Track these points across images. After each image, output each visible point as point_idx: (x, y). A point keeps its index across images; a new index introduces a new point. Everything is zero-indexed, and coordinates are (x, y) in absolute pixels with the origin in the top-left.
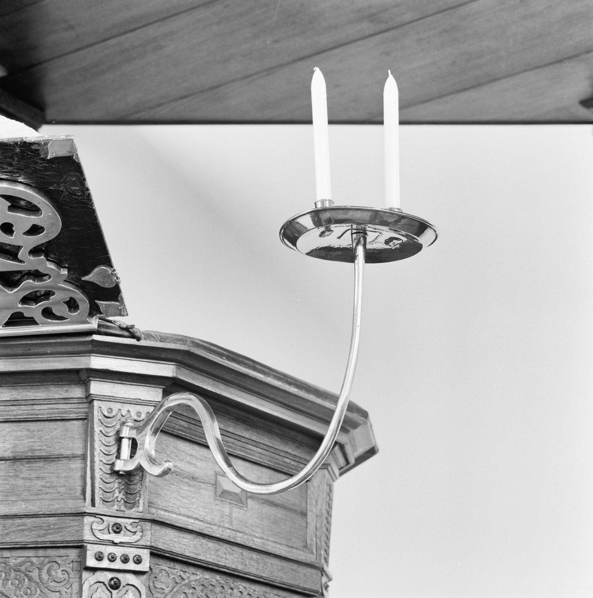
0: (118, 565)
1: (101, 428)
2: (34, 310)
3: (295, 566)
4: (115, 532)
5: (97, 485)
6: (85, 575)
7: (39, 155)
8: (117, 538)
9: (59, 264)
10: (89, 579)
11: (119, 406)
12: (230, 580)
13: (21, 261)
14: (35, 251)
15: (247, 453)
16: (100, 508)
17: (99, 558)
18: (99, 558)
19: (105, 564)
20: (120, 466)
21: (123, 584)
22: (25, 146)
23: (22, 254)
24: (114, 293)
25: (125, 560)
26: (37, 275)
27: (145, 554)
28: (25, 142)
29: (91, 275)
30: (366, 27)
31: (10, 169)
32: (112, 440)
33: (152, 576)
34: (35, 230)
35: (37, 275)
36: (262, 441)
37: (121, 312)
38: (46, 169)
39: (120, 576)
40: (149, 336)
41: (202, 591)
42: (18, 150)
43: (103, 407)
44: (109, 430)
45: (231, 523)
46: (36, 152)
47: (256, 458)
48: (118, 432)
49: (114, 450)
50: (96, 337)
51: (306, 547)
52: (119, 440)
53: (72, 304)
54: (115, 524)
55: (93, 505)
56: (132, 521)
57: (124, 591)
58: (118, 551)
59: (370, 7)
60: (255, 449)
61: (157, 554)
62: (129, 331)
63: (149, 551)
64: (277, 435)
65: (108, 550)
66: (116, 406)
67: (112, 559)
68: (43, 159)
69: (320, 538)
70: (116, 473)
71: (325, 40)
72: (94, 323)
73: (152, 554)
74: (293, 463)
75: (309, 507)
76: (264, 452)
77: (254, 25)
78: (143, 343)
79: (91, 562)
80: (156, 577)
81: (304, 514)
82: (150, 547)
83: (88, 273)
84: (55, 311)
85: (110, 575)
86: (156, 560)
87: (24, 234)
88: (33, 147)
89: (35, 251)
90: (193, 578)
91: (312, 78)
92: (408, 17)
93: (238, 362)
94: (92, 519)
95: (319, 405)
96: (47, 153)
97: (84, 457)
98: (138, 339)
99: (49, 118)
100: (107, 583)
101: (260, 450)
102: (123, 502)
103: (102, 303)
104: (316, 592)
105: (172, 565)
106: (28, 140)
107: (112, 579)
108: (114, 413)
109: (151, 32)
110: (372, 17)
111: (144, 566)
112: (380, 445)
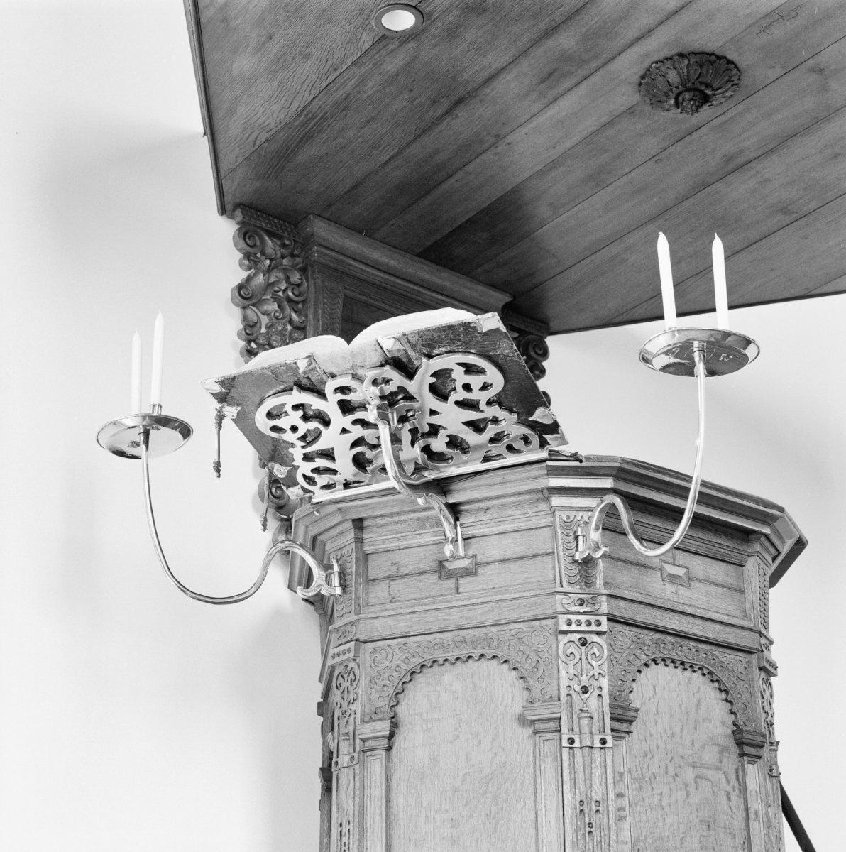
0: (583, 628)
1: (563, 531)
2: (500, 448)
3: (735, 630)
4: (580, 605)
5: (563, 571)
6: (560, 637)
7: (476, 330)
8: (582, 609)
9: (511, 411)
10: (563, 639)
11: (574, 513)
12: (679, 640)
13: (482, 411)
14: (489, 403)
15: (686, 545)
16: (566, 588)
17: (569, 624)
18: (569, 624)
19: (574, 627)
20: (578, 557)
21: (589, 642)
22: (466, 325)
23: (482, 405)
24: (554, 428)
25: (589, 624)
26: (495, 421)
27: (604, 619)
28: (465, 323)
29: (534, 416)
30: (781, 219)
31: (459, 343)
32: (572, 538)
33: (612, 636)
34: (485, 387)
35: (495, 421)
36: (697, 535)
37: (564, 442)
38: (484, 340)
39: (586, 636)
40: (588, 458)
41: (656, 647)
42: (462, 329)
43: (563, 515)
44: (568, 531)
45: (678, 598)
46: (475, 329)
47: (694, 549)
48: (575, 532)
49: (574, 545)
50: (549, 463)
51: (746, 616)
52: (577, 538)
53: (526, 440)
54: (579, 599)
55: (562, 586)
56: (592, 596)
57: (590, 647)
58: (583, 618)
59: (780, 202)
60: (692, 542)
61: (611, 619)
62: (575, 457)
63: (606, 617)
64: (711, 531)
65: (574, 617)
66: (572, 515)
67: (579, 624)
68: (480, 333)
69: (757, 608)
70: (575, 562)
71: (753, 234)
72: (544, 454)
73: (609, 619)
74: (727, 552)
75: (746, 586)
76: (701, 544)
77: (692, 231)
78: (584, 464)
79: (564, 627)
80: (615, 637)
81: (742, 592)
82: (607, 614)
83: (532, 414)
84: (515, 446)
85: (578, 636)
86: (612, 625)
87: (480, 390)
88: (472, 325)
89: (489, 403)
90: (647, 638)
91: (656, 251)
92: (813, 205)
93: (664, 474)
94: (561, 596)
95: (740, 504)
96: (481, 328)
97: (552, 553)
98: (581, 462)
99: (552, 330)
100: (576, 641)
101: (697, 543)
102: (583, 583)
103: (547, 437)
104: (756, 649)
105: (628, 628)
106: (467, 321)
107: (580, 639)
108: (571, 519)
109: (615, 249)
110: (785, 211)
111: (604, 628)
112: (807, 535)
